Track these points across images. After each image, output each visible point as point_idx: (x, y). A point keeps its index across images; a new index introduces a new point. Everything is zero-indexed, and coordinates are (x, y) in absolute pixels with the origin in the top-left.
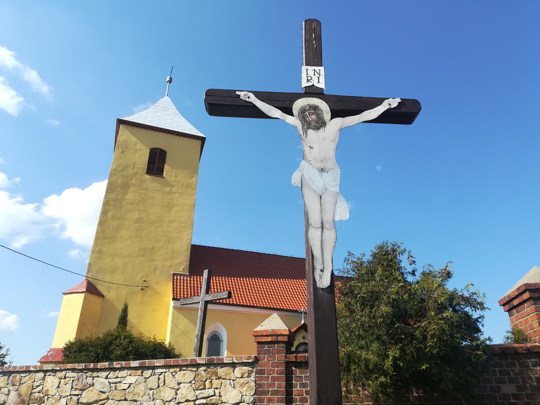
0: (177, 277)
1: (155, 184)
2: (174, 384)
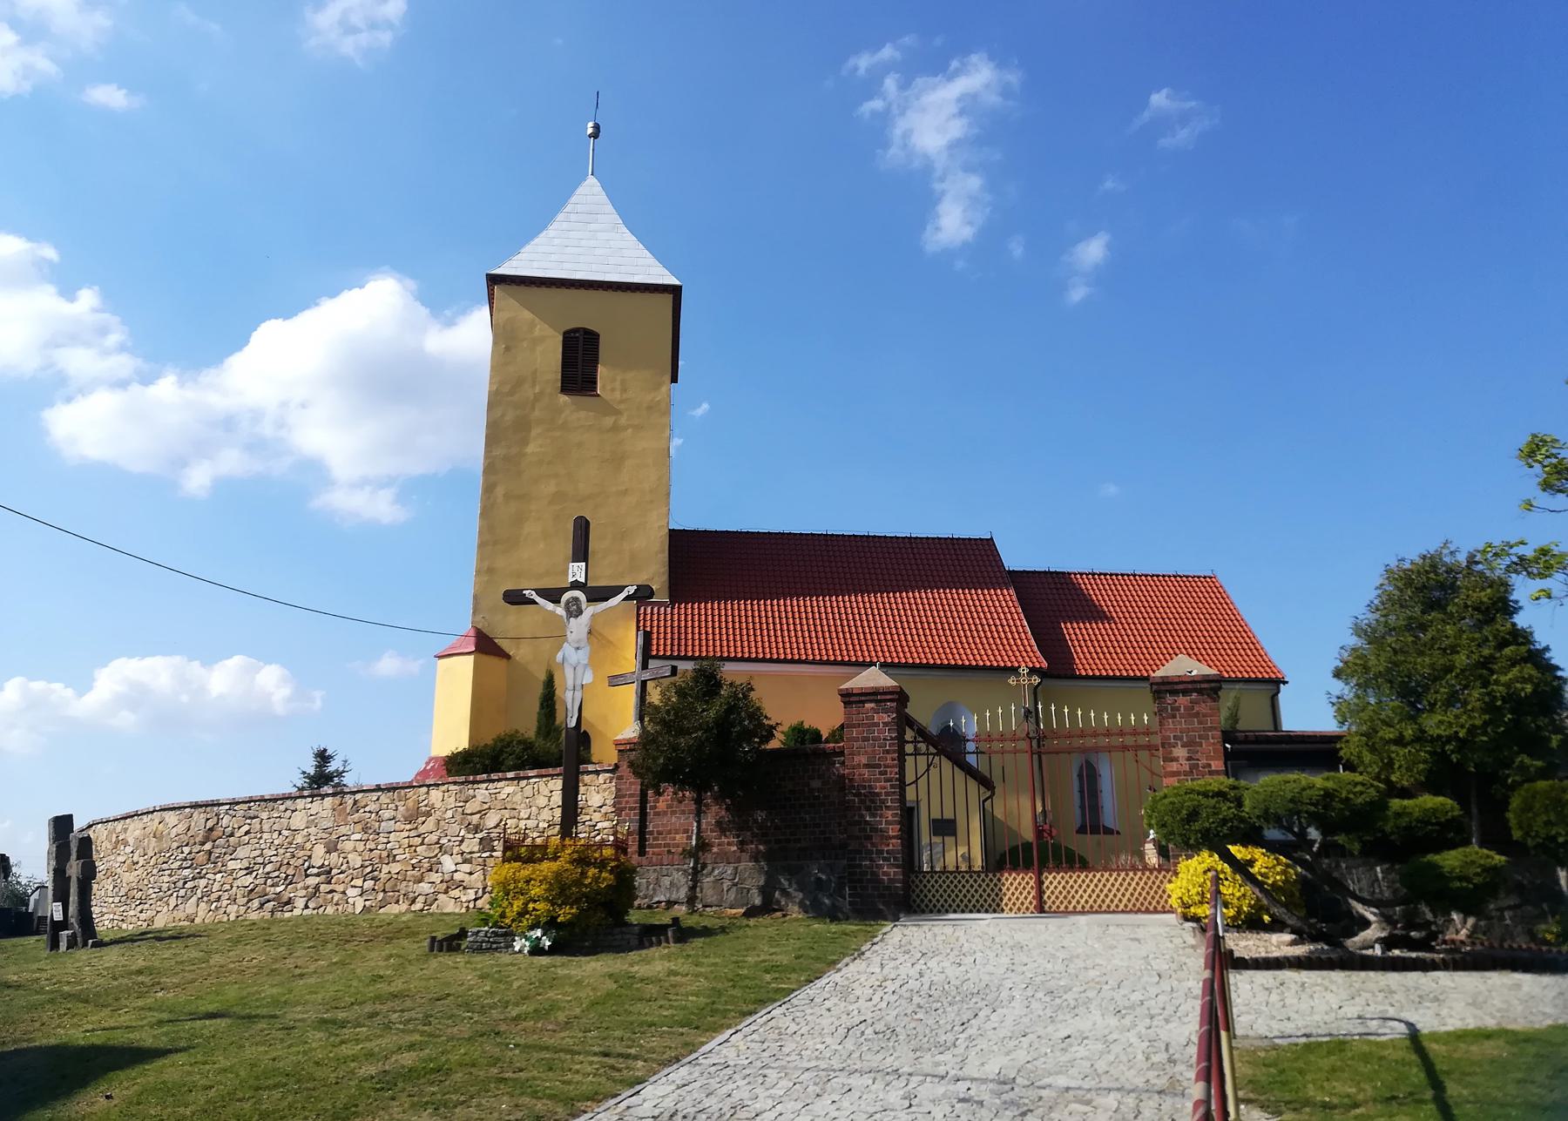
0: (645, 609)
1: (583, 414)
2: (547, 792)
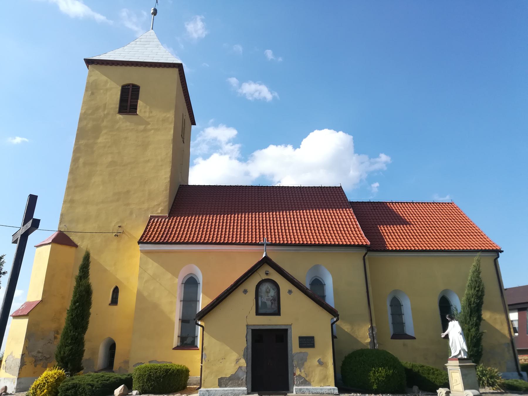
1: (128, 124)
